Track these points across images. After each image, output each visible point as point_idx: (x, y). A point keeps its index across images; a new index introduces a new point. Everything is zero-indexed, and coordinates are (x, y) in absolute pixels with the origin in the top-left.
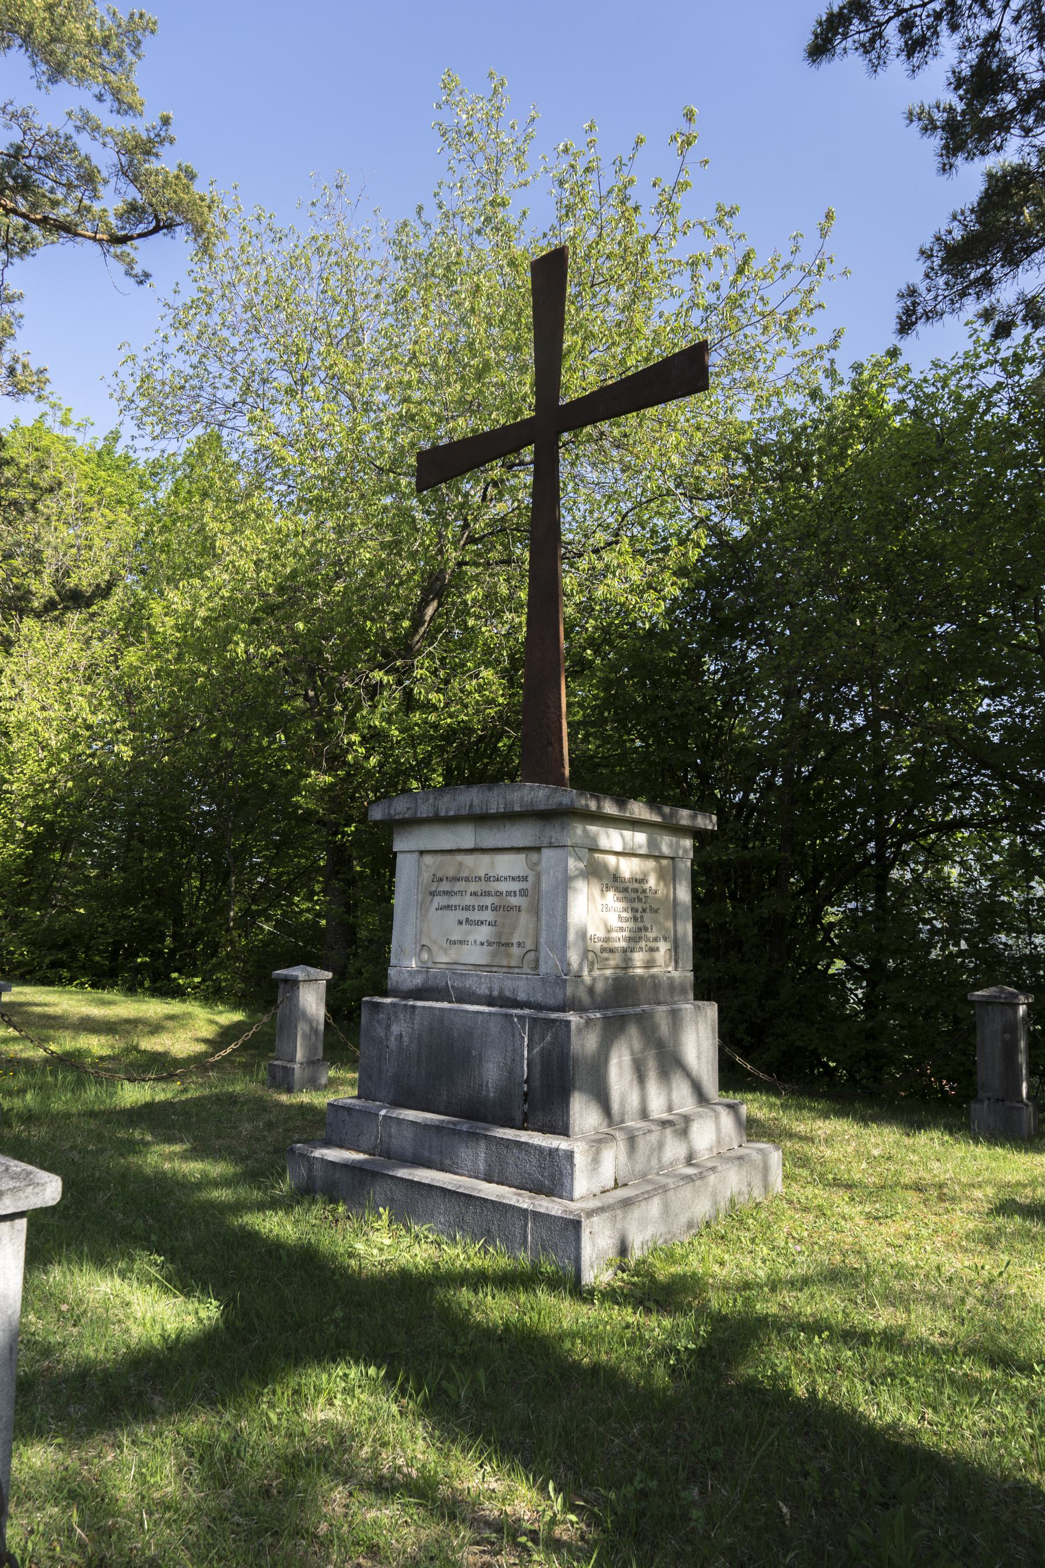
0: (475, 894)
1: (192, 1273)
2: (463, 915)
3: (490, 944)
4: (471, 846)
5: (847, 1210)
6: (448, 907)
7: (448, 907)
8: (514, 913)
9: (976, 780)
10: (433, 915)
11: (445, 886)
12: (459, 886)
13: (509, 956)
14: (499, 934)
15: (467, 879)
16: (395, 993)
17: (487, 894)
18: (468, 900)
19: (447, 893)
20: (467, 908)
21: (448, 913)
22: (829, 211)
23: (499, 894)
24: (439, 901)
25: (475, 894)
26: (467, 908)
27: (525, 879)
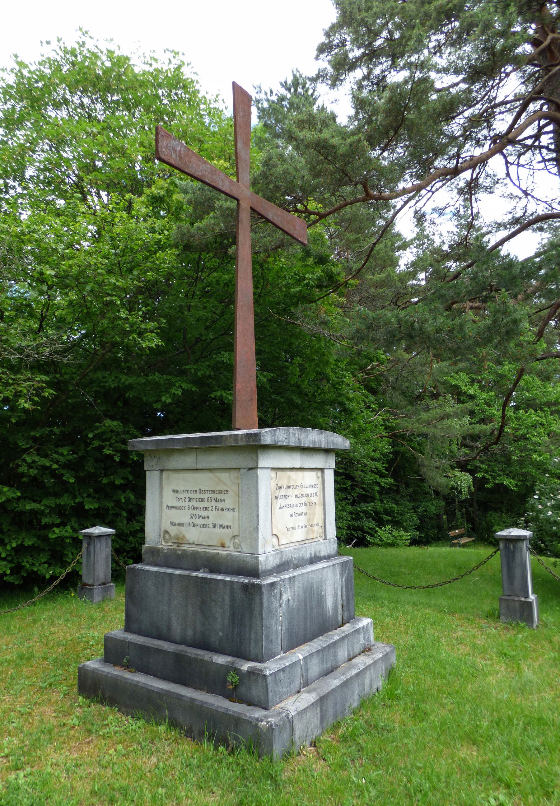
0: (297, 496)
1: (340, 767)
2: (291, 510)
3: (305, 526)
4: (299, 466)
5: (14, 184)
6: (285, 506)
7: (285, 506)
8: (313, 506)
9: (521, 723)
10: (278, 511)
11: (283, 492)
12: (290, 492)
13: (313, 532)
14: (309, 520)
15: (293, 487)
16: (270, 573)
17: (302, 496)
18: (294, 501)
19: (284, 497)
20: (294, 506)
21: (285, 510)
22: (548, 795)
23: (307, 495)
24: (281, 502)
25: (297, 496)
26: (294, 506)
27: (316, 486)
